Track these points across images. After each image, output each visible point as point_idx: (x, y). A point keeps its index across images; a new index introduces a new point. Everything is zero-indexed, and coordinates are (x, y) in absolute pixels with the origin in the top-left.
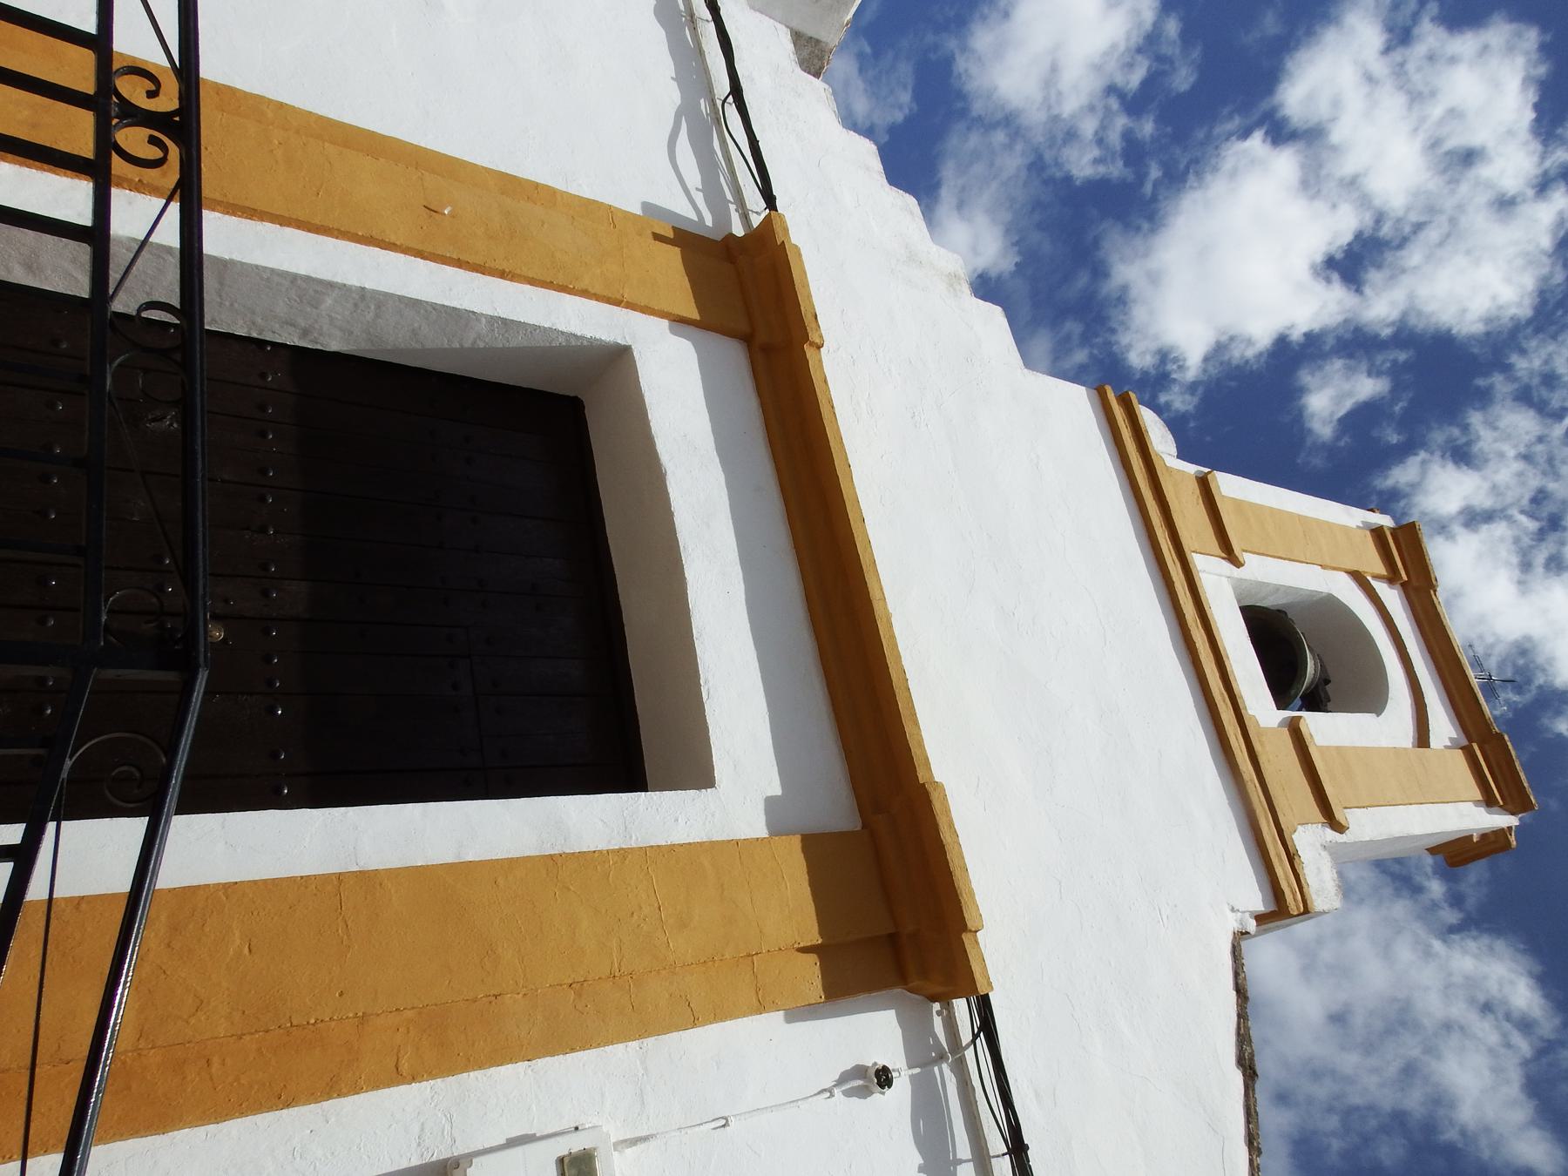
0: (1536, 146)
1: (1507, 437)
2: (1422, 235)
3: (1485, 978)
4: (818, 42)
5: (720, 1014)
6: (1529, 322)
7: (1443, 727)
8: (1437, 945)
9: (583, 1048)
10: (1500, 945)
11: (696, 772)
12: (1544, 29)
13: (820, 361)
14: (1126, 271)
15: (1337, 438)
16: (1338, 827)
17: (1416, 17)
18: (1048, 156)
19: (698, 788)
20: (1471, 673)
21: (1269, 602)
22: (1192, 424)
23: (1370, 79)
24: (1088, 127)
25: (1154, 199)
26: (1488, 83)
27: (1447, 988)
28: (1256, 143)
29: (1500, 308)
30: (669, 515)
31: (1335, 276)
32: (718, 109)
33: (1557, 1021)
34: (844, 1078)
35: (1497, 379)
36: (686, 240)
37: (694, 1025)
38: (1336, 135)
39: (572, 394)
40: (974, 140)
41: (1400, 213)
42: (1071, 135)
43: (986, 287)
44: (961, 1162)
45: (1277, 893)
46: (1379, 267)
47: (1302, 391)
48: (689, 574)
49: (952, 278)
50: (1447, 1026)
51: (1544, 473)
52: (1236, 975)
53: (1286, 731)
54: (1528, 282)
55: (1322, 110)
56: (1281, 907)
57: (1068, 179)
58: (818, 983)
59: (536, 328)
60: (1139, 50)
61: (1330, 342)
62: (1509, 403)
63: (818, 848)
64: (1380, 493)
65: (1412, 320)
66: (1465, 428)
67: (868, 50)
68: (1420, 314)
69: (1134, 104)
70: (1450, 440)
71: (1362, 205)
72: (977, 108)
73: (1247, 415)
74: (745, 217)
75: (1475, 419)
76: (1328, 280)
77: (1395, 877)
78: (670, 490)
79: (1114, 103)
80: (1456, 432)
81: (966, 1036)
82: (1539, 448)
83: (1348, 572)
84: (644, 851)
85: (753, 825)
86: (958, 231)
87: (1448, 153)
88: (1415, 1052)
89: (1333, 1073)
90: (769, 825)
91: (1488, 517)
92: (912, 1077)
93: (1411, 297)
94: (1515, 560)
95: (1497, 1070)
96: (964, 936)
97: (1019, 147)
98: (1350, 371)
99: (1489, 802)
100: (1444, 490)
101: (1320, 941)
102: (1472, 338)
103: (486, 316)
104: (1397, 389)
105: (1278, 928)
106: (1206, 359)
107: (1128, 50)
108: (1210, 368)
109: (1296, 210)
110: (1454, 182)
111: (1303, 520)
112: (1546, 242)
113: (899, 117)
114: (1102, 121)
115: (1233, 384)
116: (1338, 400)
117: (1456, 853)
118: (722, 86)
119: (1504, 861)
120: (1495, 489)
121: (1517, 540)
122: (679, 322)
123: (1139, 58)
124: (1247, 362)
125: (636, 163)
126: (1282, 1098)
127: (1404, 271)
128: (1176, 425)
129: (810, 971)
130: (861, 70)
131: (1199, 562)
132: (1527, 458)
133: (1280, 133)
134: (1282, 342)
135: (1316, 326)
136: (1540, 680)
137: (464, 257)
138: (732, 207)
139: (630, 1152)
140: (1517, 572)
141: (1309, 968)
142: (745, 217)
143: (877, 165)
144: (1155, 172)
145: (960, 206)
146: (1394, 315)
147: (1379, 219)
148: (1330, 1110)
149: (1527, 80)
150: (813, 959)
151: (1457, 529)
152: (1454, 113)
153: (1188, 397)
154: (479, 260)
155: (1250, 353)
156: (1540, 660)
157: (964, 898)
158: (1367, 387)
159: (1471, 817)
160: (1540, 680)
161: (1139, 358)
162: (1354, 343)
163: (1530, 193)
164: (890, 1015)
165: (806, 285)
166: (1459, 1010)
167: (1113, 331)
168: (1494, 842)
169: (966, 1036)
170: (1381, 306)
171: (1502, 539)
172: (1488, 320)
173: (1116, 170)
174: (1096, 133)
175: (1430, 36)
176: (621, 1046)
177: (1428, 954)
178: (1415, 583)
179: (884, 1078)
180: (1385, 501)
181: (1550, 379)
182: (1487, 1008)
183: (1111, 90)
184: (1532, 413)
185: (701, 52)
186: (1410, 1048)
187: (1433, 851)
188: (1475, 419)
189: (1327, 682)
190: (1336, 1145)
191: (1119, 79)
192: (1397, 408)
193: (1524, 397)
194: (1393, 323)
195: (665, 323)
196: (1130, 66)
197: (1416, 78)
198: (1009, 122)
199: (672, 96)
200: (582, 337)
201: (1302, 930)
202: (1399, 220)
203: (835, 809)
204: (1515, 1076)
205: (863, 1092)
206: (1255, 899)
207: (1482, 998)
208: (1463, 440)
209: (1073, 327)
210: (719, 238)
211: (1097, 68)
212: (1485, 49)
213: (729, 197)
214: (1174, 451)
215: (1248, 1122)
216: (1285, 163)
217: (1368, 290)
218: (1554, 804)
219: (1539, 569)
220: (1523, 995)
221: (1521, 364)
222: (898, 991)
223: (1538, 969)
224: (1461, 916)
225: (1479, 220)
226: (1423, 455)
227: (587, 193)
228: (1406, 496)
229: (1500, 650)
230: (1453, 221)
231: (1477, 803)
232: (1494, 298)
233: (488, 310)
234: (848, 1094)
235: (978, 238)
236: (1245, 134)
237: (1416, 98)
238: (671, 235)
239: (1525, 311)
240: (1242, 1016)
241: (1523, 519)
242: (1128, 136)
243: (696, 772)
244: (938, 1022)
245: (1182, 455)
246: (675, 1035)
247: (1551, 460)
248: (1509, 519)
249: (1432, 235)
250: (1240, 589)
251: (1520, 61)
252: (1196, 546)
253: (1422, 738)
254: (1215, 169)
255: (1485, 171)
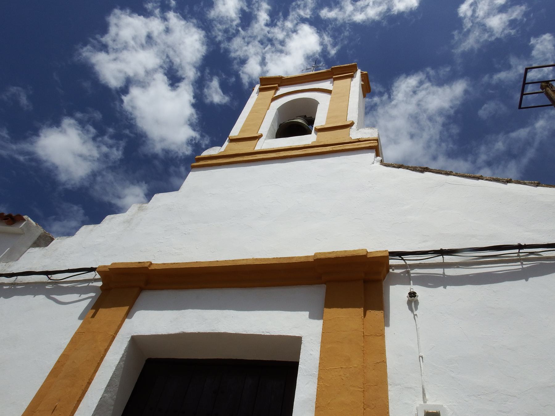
0: (152, 18)
1: (241, 47)
2: (171, 56)
3: (405, 91)
4: (40, 236)
5: (382, 352)
6: (206, 32)
7: (326, 85)
8: (394, 103)
9: (388, 408)
10: (396, 84)
11: (295, 343)
12: (115, 7)
13: (156, 264)
14: (158, 148)
15: (230, 96)
16: (352, 124)
17: (100, 42)
18: (110, 164)
19: (301, 343)
20: (311, 73)
21: (276, 128)
22: (215, 139)
23: (115, 60)
24: (105, 149)
25: (136, 134)
26: (128, 26)
27: (406, 102)
28: (126, 99)
29: (200, 40)
30: (199, 334)
31: (177, 84)
32: (50, 284)
33: (421, 73)
34: (411, 309)
35: (222, 45)
36: (97, 306)
37: (386, 362)
38: (131, 74)
39: (144, 362)
40: (97, 187)
41: (162, 61)
42: (106, 156)
43: (149, 196)
44: (444, 272)
45: (370, 148)
46: (177, 71)
47: (212, 103)
48: (222, 330)
49: (140, 209)
50: (418, 105)
51: (254, 39)
52: (394, 167)
53: (319, 133)
54: (194, 30)
55: (121, 76)
56: (375, 148)
57: (121, 160)
58: (377, 312)
59: (114, 373)
60: (83, 127)
61: (197, 91)
62: (230, 44)
63: (330, 303)
64: (250, 87)
65: (197, 65)
66: (235, 59)
67: (54, 217)
68: (196, 63)
69: (101, 132)
70: (238, 64)
71: (156, 71)
72: (86, 184)
73: (214, 122)
74: (96, 280)
75: (233, 55)
76: (178, 86)
77: (371, 110)
78: (190, 331)
79: (99, 139)
80: (235, 62)
81: (402, 262)
82: (246, 40)
83: (272, 102)
84: (321, 370)
85: (318, 325)
86: (129, 200)
87: (146, 42)
88: (425, 116)
89: (429, 141)
90: (318, 319)
91: (264, 59)
92: (413, 284)
93: (189, 63)
94: (279, 54)
95: (434, 94)
96: (368, 257)
97: (104, 173)
98: (208, 87)
99: (352, 77)
100: (253, 69)
101: (387, 136)
102: (207, 50)
103: (104, 393)
104: (218, 75)
105: (381, 149)
106: (194, 130)
107: (82, 131)
108: (197, 129)
109: (152, 91)
110: (156, 44)
111: (252, 112)
112: (183, 22)
113: (82, 211)
114: (104, 144)
115: (204, 123)
116: (217, 92)
117: (366, 90)
118: (44, 278)
119: (371, 77)
120: (256, 54)
121: (273, 52)
122: (128, 315)
123: (86, 127)
124: (198, 118)
125: (65, 317)
126: (435, 158)
127: (181, 64)
128: (213, 144)
129: (371, 314)
130: (60, 220)
131: (258, 148)
132: (248, 43)
133: (125, 90)
134: (194, 106)
135: (192, 94)
136: (317, 56)
137: (77, 398)
138: (91, 284)
139: (427, 397)
140: (283, 54)
141: (396, 142)
142: (96, 280)
143: (91, 227)
144: (127, 132)
145: (119, 197)
146: (194, 70)
147: (161, 67)
148: (440, 145)
149: (130, 15)
150: (368, 312)
151: (265, 69)
152: (134, 38)
153: (205, 139)
154: (80, 392)
155: (195, 116)
156: (311, 54)
157: (355, 254)
158: (215, 83)
159: (355, 84)
160: (317, 56)
161: (188, 151)
162: (200, 85)
163: (166, 23)
164: (391, 287)
165: (127, 263)
166: (414, 100)
167: (177, 157)
168: (364, 78)
169: (402, 262)
170: (191, 73)
171: (271, 56)
172: (203, 44)
173: (122, 144)
174: (108, 147)
175: (107, 39)
176: (389, 393)
177: (396, 106)
178: (279, 83)
179: (412, 295)
180: (252, 86)
181: (226, 31)
182: (415, 92)
183: (94, 139)
184: (235, 39)
185: (28, 283)
186: (423, 117)
187: (364, 96)
188: (233, 55)
189: (305, 116)
190: (451, 145)
191: (91, 135)
192: (224, 77)
193: (229, 39)
194: (197, 71)
195: (127, 320)
196: (88, 131)
197: (119, 46)
198: (94, 175)
199: (41, 298)
200: (123, 355)
201: (383, 141)
202: (164, 62)
203: (318, 293)
204: (435, 89)
205: (417, 303)
206: (371, 155)
207: (411, 93)
208: (238, 60)
209: (172, 169)
210: (100, 292)
211: (85, 142)
212: (116, 25)
213: (86, 285)
214: (219, 148)
215: (441, 174)
216: (135, 92)
217: (184, 76)
218: (356, 60)
219: (283, 48)
220: (412, 81)
221: (219, 38)
222: (384, 283)
223: (404, 75)
224: (386, 93)
225: (170, 39)
226: (240, 72)
227: (68, 341)
228: (252, 80)
229: (305, 64)
230: (169, 46)
231: (352, 80)
232: (196, 40)
233: (102, 392)
234: (416, 309)
235: (133, 194)
236: (122, 101)
237: (126, 47)
238: (94, 311)
239: (202, 33)
240: (407, 168)
241: (267, 49)
242: (111, 137)
243: (295, 343)
244: (397, 271)
245: (221, 145)
246: (388, 371)
247: (250, 37)
248: (265, 53)
249: (171, 53)
250: (270, 137)
251: (123, 16)
252: (253, 148)
253: (329, 92)
254: (131, 114)
255: (155, 34)
